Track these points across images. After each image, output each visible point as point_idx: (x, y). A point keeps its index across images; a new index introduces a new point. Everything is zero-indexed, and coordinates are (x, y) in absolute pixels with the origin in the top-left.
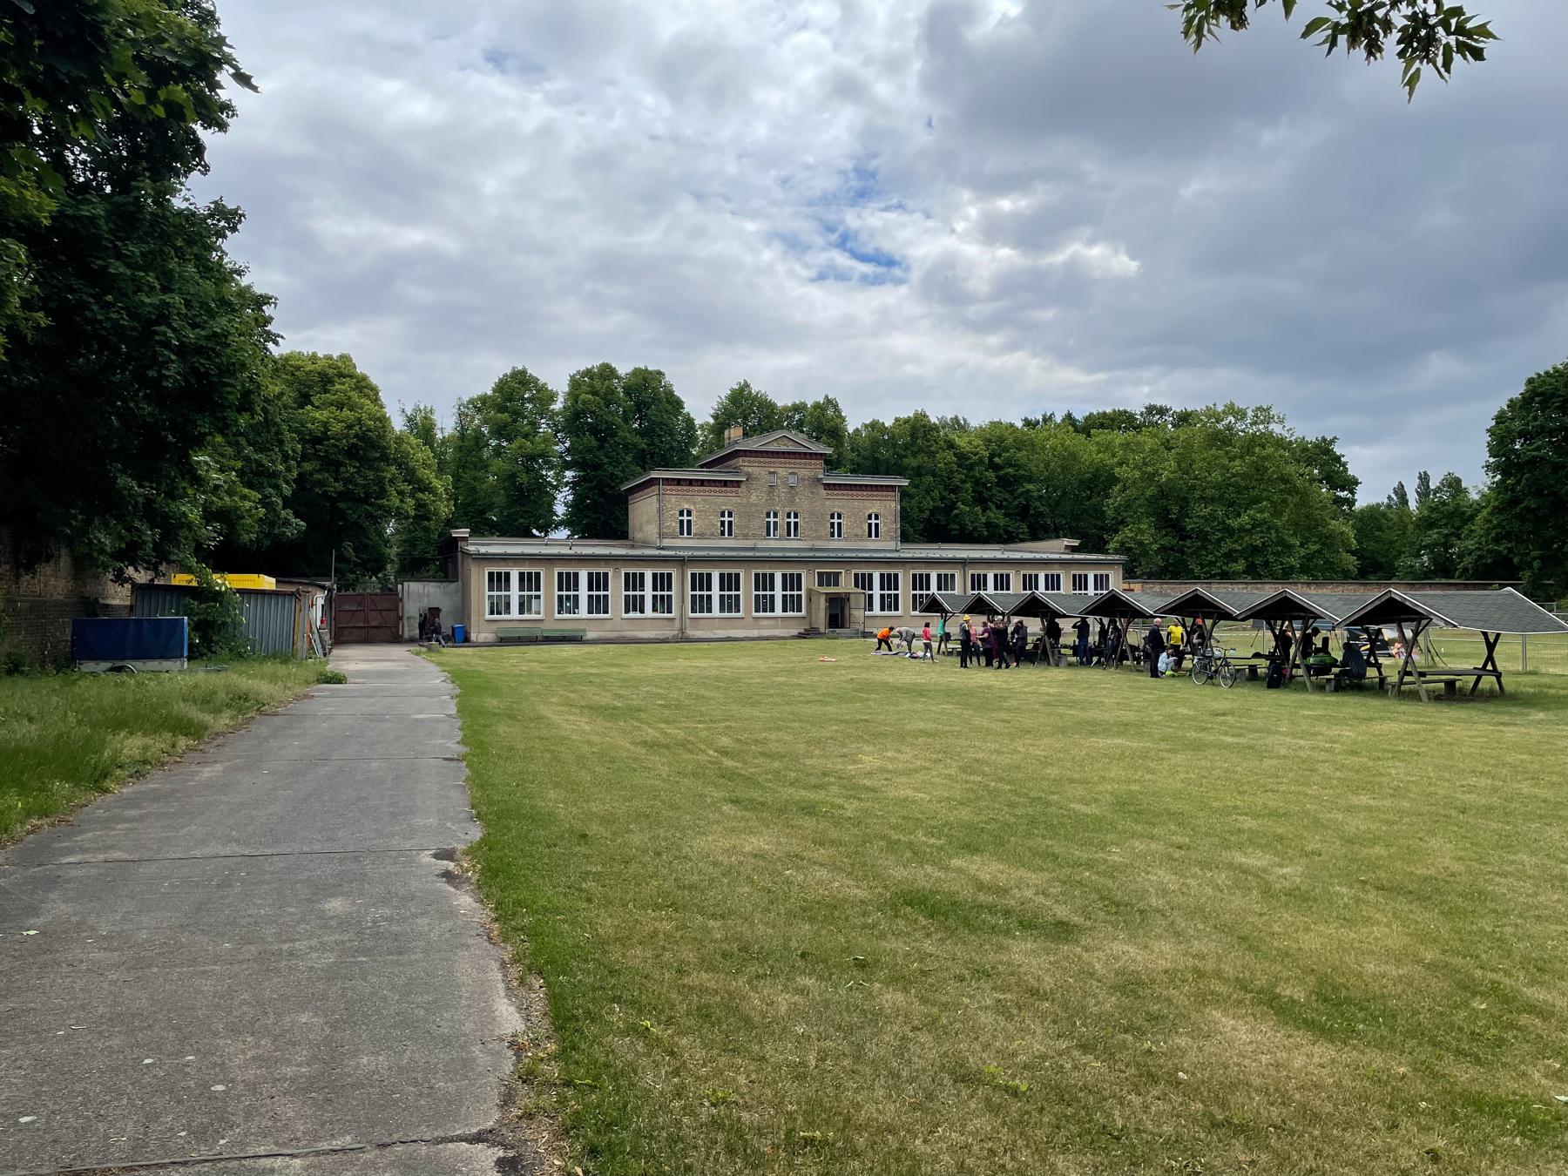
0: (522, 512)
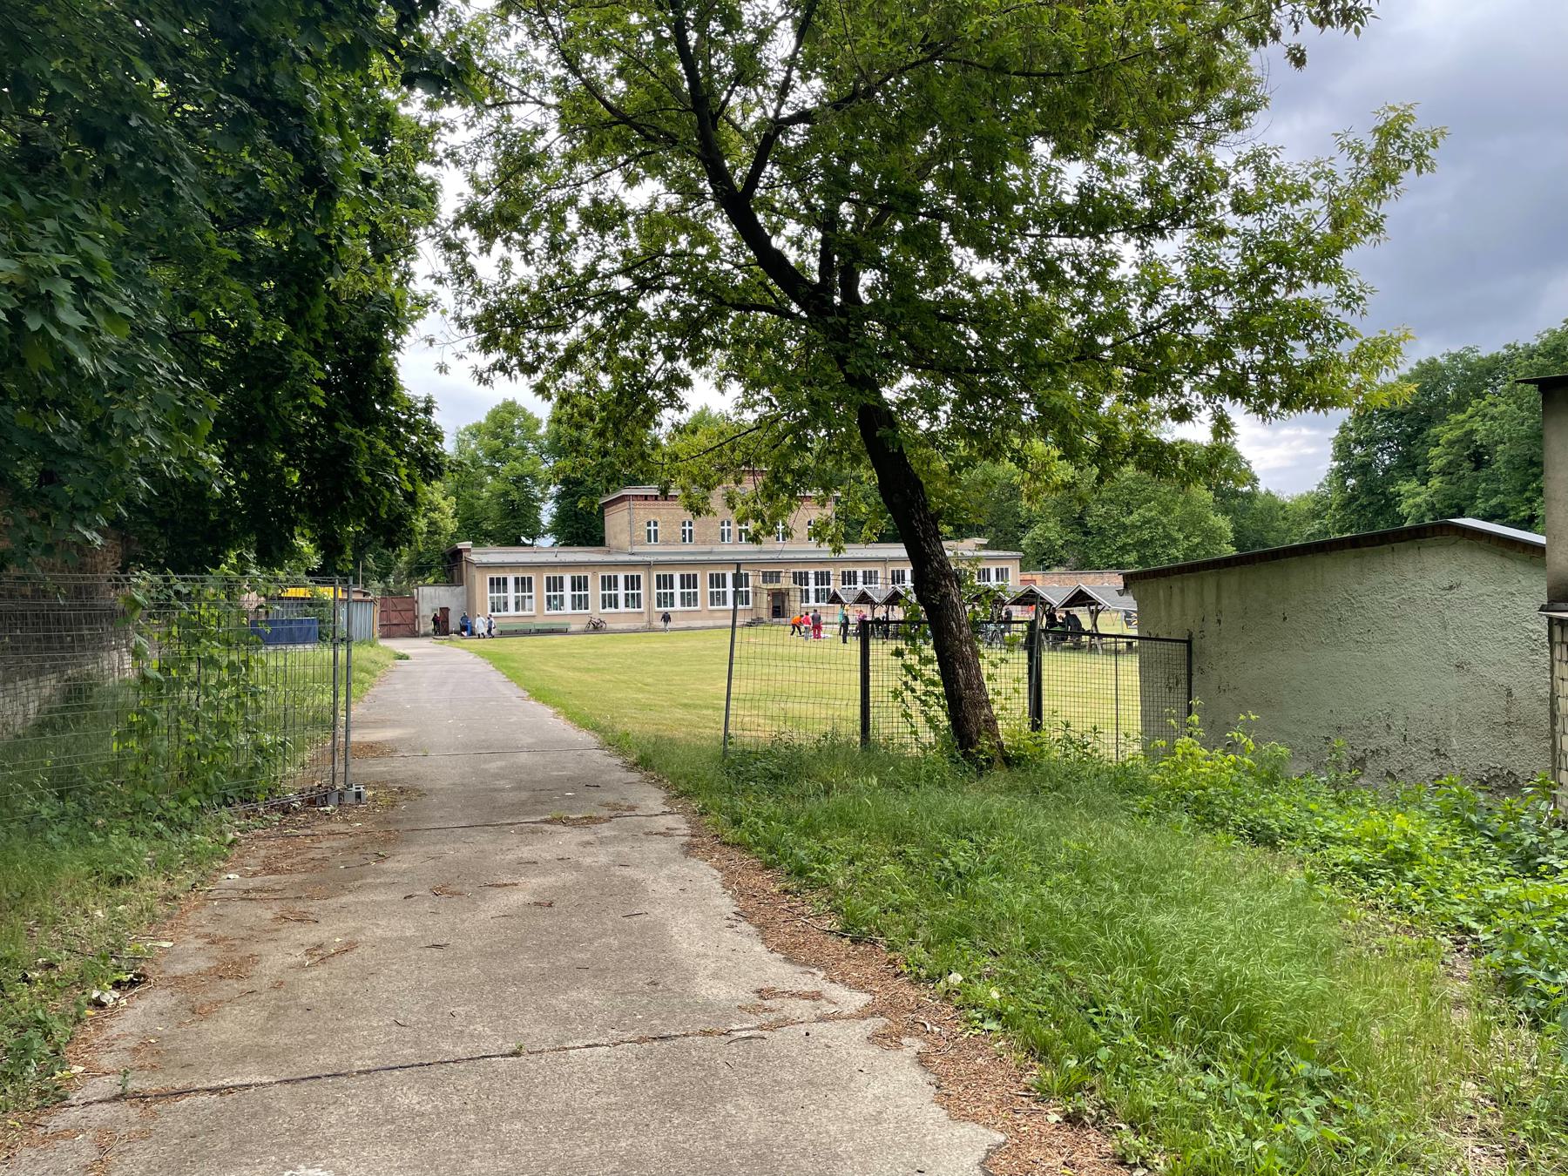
0: (514, 524)
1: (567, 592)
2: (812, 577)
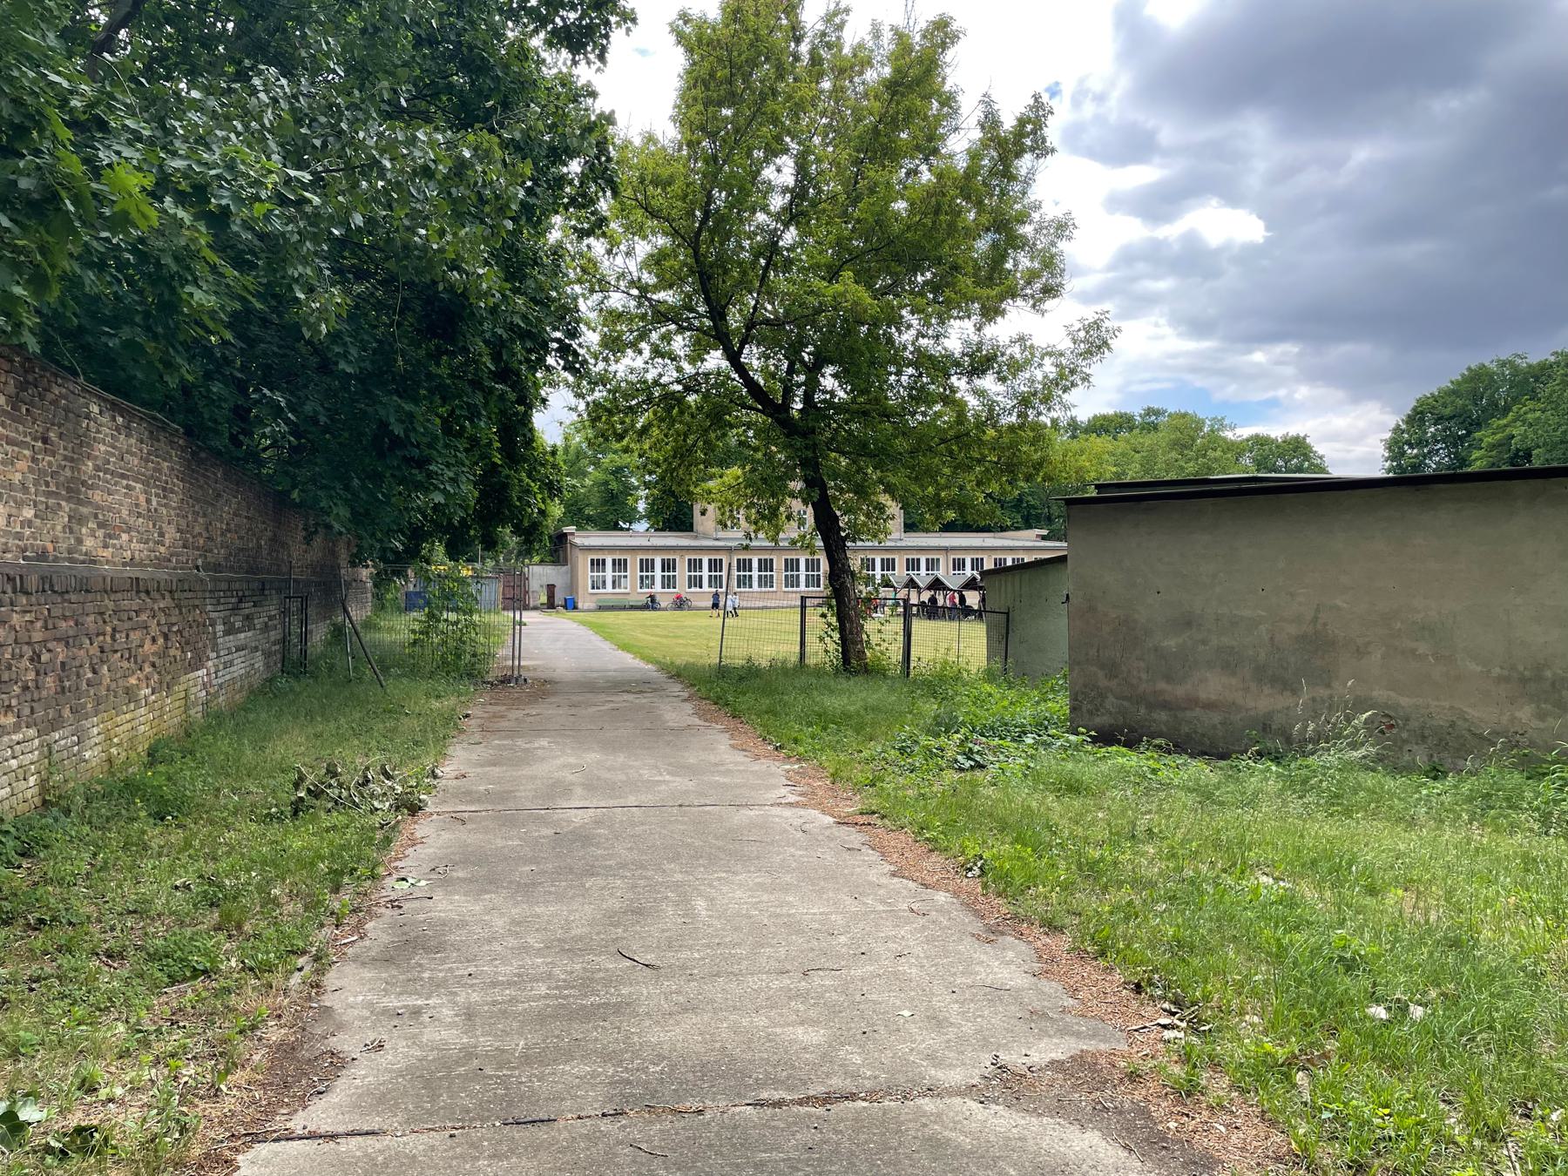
0: (613, 513)
1: (658, 573)
2: (755, 565)
